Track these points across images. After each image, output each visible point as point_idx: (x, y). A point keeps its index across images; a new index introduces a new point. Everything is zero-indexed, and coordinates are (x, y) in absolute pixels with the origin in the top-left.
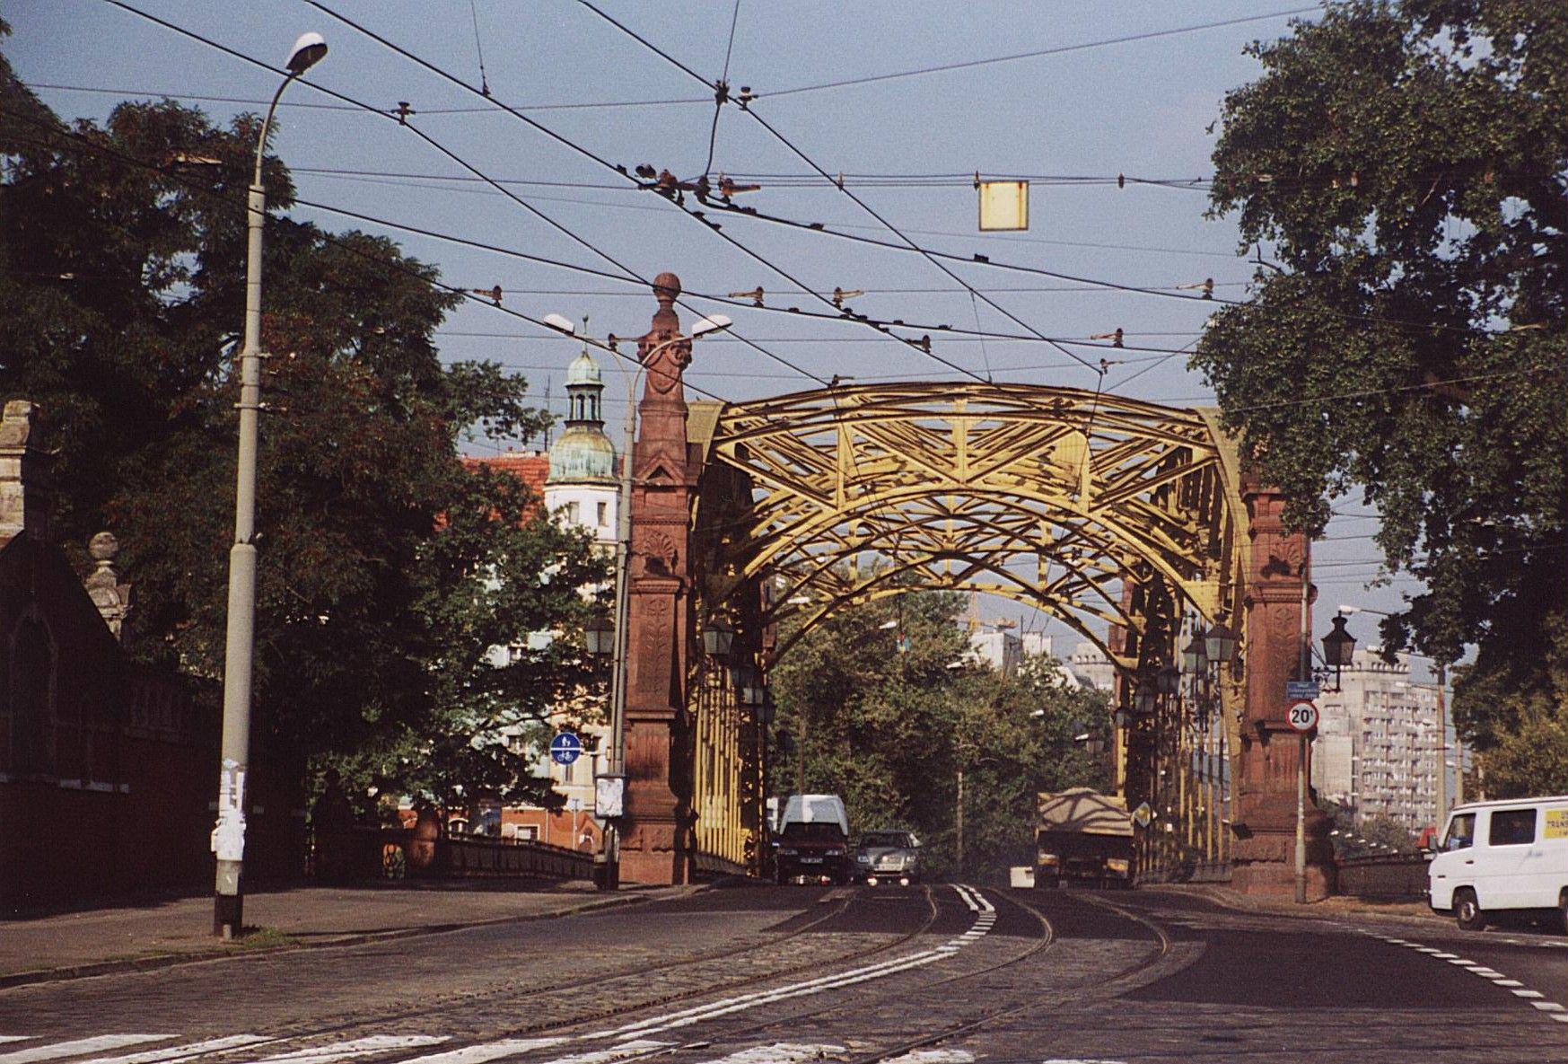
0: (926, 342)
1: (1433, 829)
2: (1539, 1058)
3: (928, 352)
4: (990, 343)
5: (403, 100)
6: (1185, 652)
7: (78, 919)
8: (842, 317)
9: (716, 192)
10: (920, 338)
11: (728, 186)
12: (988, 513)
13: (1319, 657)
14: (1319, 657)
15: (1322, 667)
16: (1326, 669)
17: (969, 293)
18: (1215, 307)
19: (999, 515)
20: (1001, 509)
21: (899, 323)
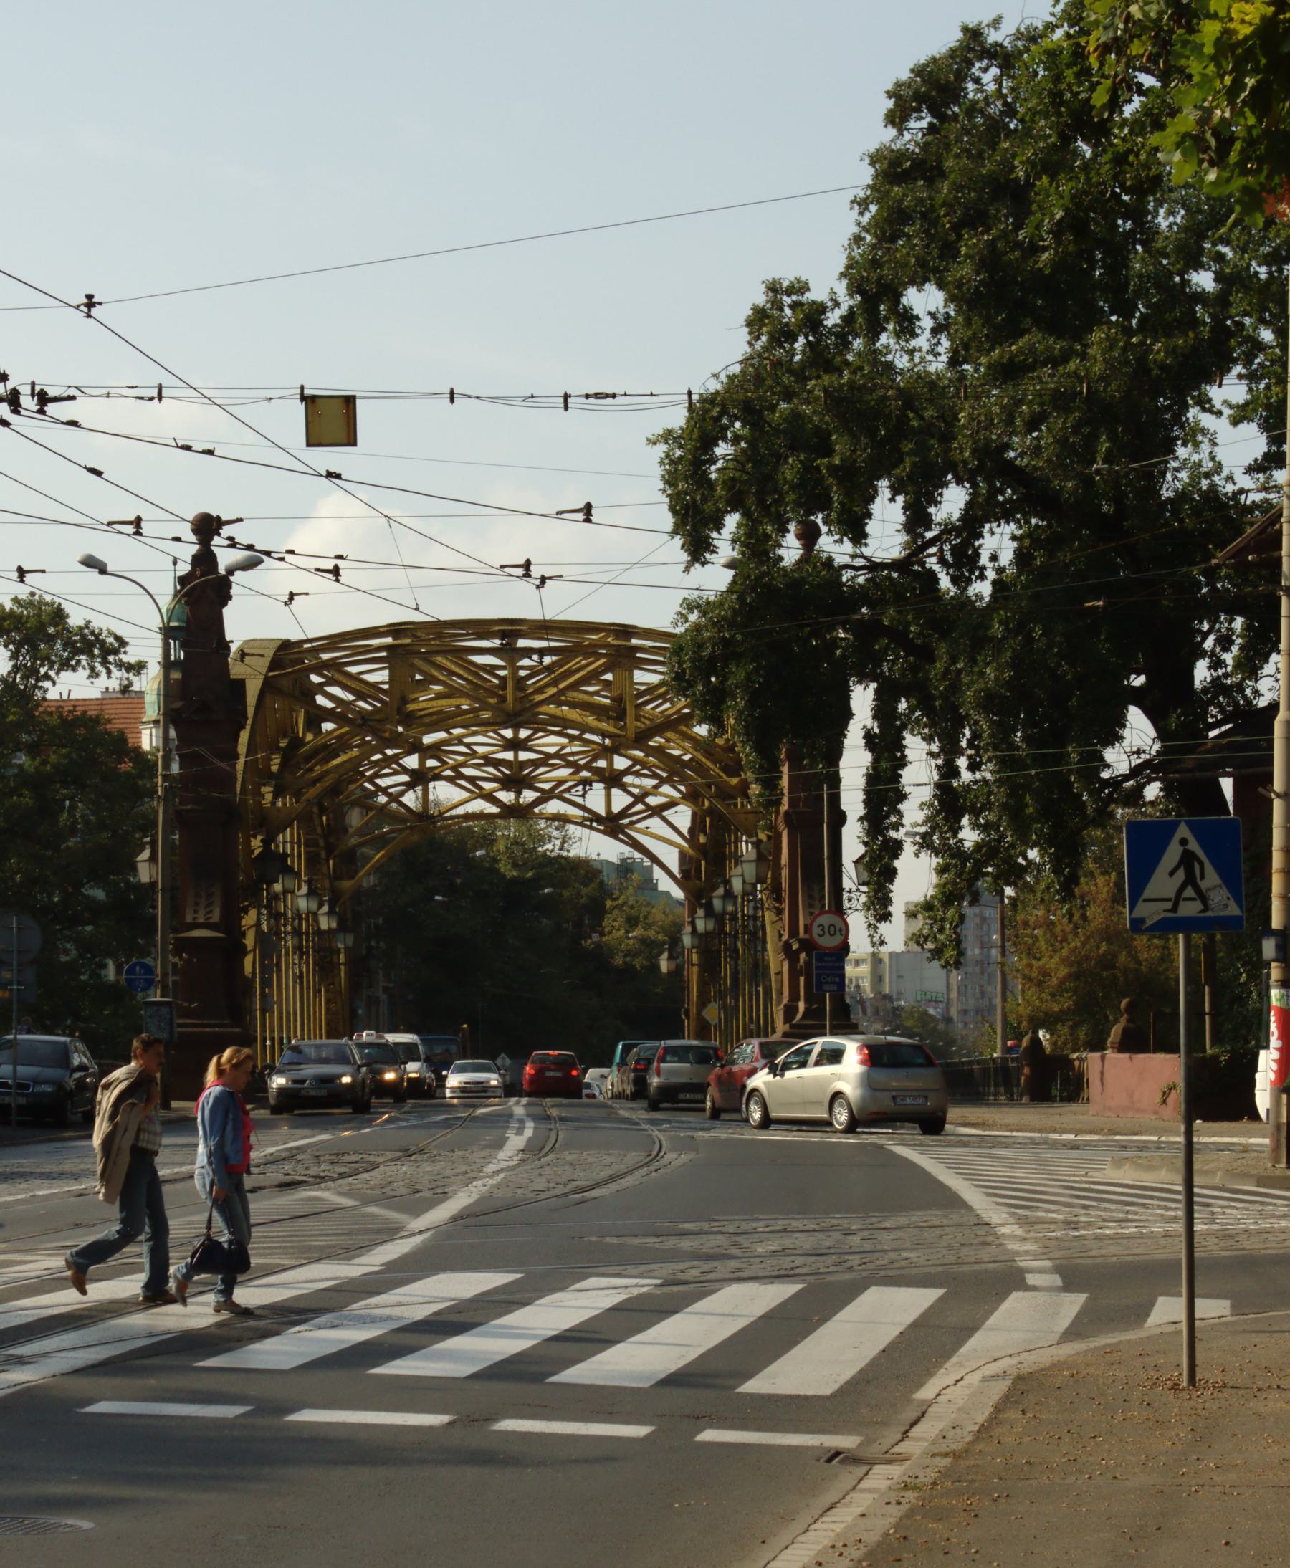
0: (336, 571)
1: (871, 156)
2: (1285, 1127)
3: (338, 581)
4: (409, 571)
5: (327, 384)
6: (709, 1084)
7: (634, 1385)
8: (229, 546)
9: (28, 402)
10: (330, 567)
11: (43, 399)
12: (552, 745)
13: (851, 878)
14: (851, 878)
15: (854, 888)
16: (858, 890)
17: (384, 520)
18: (23, 592)
19: (563, 747)
20: (565, 741)
21: (291, 552)
